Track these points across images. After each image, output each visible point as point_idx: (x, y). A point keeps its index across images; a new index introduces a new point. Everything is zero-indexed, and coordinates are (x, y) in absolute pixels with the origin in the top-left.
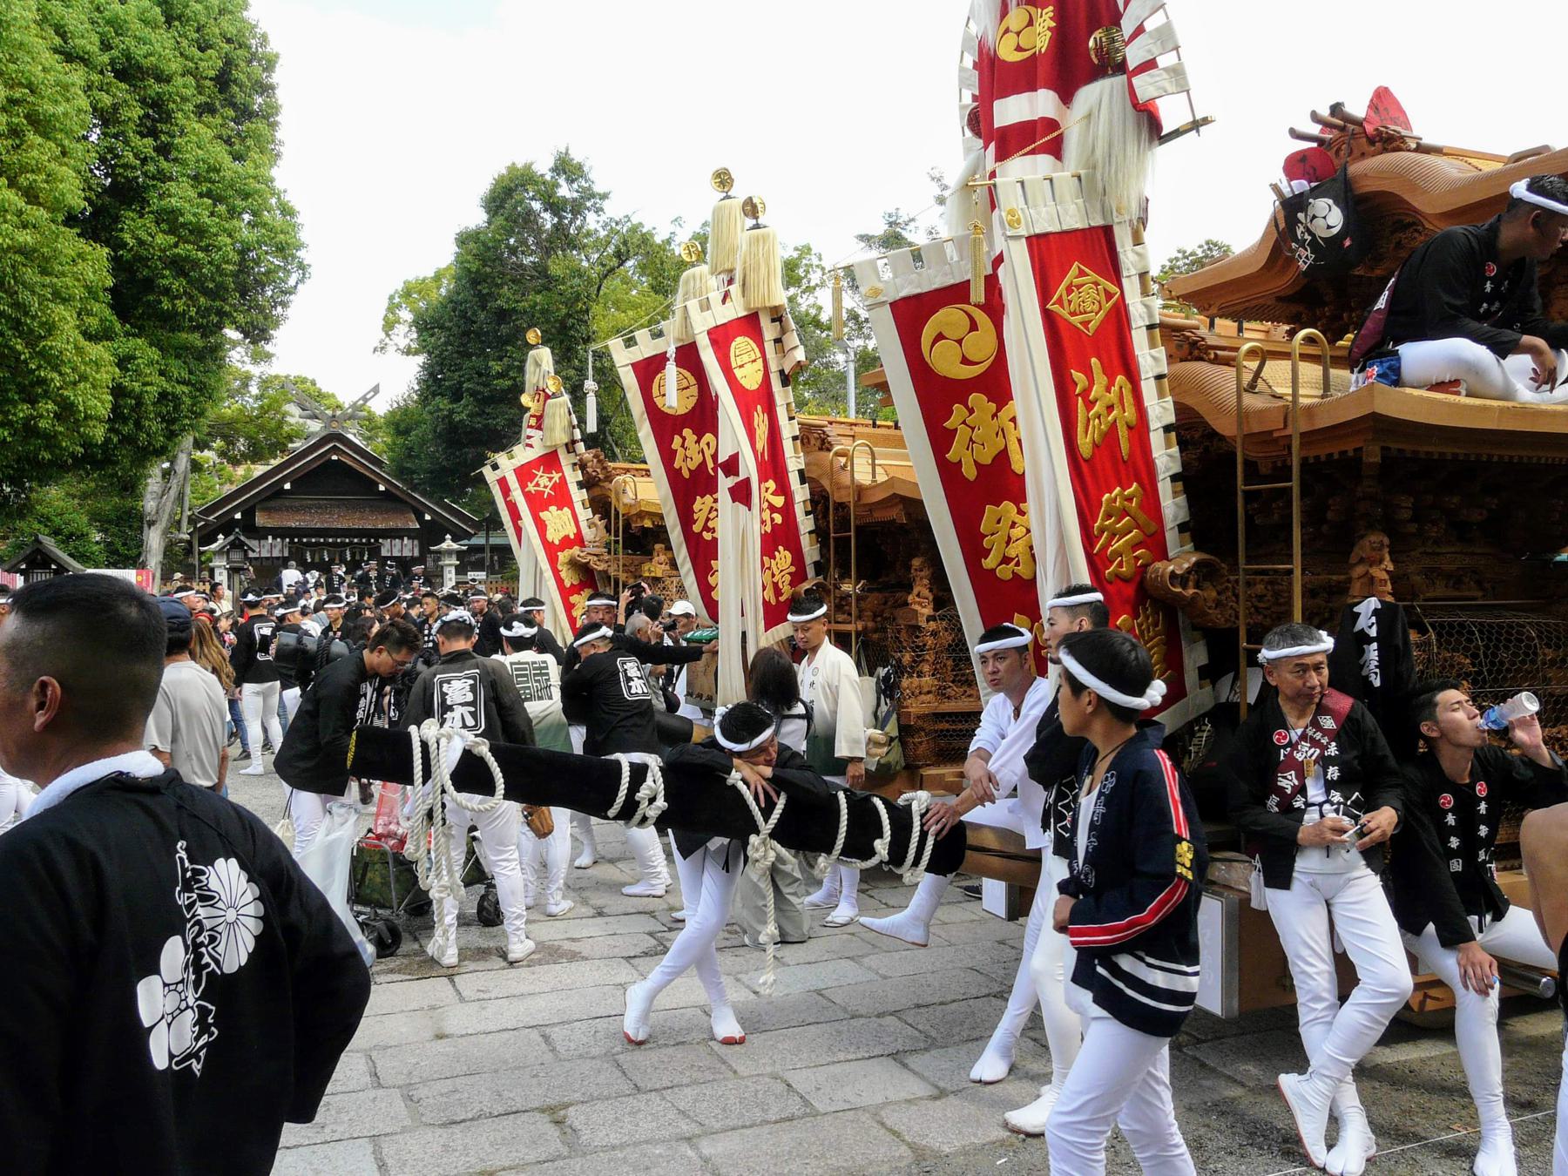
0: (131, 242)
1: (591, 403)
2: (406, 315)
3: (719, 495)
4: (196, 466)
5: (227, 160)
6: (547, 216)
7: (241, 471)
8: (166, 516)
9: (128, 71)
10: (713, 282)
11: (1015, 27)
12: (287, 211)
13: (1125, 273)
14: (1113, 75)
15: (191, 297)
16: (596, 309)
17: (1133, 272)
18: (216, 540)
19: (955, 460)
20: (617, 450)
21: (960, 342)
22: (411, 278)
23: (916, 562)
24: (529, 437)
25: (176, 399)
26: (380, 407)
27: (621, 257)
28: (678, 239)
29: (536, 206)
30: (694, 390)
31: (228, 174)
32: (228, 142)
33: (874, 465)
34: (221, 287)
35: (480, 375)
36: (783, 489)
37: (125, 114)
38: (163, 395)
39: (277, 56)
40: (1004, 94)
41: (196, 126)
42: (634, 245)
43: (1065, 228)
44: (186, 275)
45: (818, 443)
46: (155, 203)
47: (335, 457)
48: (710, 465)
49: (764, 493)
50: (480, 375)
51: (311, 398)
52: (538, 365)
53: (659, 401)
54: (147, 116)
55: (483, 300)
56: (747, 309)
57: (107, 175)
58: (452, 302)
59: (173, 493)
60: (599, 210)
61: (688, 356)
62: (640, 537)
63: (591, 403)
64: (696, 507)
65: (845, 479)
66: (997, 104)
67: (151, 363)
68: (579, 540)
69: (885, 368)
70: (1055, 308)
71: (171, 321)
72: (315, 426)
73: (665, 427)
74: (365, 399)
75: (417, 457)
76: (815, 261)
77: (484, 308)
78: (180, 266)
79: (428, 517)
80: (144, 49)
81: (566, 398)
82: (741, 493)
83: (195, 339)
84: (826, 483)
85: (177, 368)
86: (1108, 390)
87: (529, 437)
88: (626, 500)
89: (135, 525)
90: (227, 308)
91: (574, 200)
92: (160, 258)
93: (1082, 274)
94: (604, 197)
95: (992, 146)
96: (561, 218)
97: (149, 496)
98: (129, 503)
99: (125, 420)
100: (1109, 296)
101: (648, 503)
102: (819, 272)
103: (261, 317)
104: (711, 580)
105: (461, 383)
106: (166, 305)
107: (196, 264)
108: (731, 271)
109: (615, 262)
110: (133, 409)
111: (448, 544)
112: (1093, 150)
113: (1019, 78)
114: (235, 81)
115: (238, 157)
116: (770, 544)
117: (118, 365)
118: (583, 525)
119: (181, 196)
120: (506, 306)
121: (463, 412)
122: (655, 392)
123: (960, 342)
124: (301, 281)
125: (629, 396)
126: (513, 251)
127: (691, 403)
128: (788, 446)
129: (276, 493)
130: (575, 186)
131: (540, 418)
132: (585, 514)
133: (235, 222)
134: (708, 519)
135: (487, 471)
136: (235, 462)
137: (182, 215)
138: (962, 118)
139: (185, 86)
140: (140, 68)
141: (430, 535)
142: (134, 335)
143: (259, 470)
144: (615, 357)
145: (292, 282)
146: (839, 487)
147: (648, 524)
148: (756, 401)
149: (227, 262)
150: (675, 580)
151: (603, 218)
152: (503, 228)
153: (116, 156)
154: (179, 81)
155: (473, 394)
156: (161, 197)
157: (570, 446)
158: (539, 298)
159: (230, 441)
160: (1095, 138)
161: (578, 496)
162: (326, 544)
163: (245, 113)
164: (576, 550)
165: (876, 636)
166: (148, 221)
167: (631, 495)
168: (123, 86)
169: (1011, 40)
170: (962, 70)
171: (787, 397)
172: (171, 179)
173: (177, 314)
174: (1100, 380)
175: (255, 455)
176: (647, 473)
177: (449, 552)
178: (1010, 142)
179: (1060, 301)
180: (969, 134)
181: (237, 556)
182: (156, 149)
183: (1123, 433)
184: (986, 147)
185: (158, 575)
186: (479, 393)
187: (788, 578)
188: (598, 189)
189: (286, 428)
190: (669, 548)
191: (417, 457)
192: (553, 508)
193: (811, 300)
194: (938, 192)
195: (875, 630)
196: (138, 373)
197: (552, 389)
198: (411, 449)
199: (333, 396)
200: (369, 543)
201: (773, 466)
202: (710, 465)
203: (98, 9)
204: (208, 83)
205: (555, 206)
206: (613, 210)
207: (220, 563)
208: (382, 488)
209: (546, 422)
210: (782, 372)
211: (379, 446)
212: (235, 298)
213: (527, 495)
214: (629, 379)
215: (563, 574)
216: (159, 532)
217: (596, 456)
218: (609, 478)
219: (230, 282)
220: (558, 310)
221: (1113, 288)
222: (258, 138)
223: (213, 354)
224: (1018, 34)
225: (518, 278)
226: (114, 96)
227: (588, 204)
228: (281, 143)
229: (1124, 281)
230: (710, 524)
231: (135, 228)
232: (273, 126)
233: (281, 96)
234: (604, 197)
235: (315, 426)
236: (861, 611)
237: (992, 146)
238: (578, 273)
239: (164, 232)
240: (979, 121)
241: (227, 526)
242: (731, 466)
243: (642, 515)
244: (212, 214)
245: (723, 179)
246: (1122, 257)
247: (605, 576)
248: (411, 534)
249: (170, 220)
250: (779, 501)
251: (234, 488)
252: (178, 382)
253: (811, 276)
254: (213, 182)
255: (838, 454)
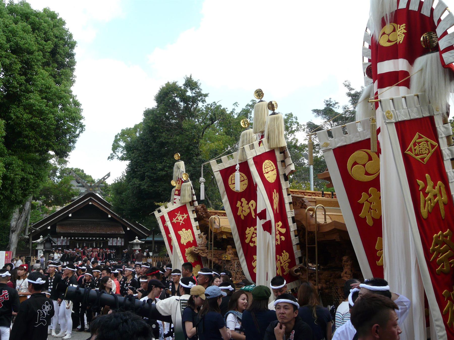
0: (14, 117)
1: (202, 187)
2: (122, 144)
3: (257, 227)
4: (33, 207)
5: (53, 84)
6: (182, 104)
7: (51, 209)
8: (19, 229)
9: (17, 50)
10: (255, 136)
11: (387, 32)
12: (77, 104)
13: (440, 136)
14: (432, 52)
15: (36, 139)
16: (201, 141)
17: (444, 135)
18: (39, 238)
19: (363, 217)
20: (210, 202)
21: (364, 165)
22: (124, 128)
23: (345, 258)
24: (175, 199)
25: (28, 180)
26: (110, 182)
27: (212, 120)
28: (236, 112)
29: (177, 99)
30: (246, 182)
31: (54, 90)
32: (54, 77)
33: (325, 215)
34: (49, 134)
35: (152, 169)
36: (285, 225)
37: (14, 67)
38: (23, 179)
39: (75, 43)
40: (383, 60)
41: (42, 71)
42: (217, 114)
43: (412, 118)
44: (35, 130)
45: (300, 205)
46: (24, 101)
47: (90, 203)
48: (253, 214)
49: (277, 227)
50: (152, 169)
51: (80, 176)
52: (179, 168)
53: (231, 187)
54: (23, 67)
55: (154, 138)
56: (270, 148)
57: (5, 91)
58: (141, 138)
59: (23, 218)
60: (203, 101)
61: (244, 167)
62: (221, 242)
63: (202, 187)
64: (247, 232)
65: (313, 221)
66: (379, 64)
67: (19, 166)
68: (194, 243)
69: (329, 171)
70: (409, 153)
71: (27, 148)
72: (83, 190)
73: (234, 197)
74: (104, 179)
75: (125, 204)
76: (294, 120)
77: (155, 141)
78: (32, 126)
79: (128, 229)
80: (23, 42)
81: (190, 182)
82: (267, 227)
83: (37, 155)
84: (304, 223)
85: (29, 168)
86: (434, 188)
87: (175, 199)
88: (215, 227)
89: (6, 232)
90: (51, 143)
91: (193, 97)
92: (25, 123)
93: (420, 137)
94: (206, 95)
95: (376, 82)
96: (188, 104)
97: (13, 220)
98: (4, 222)
99: (6, 189)
100: (433, 146)
101: (225, 228)
102: (296, 125)
103: (64, 147)
104: (253, 264)
105: (144, 173)
106: (27, 142)
107: (39, 126)
108: (263, 132)
109: (209, 122)
110: (10, 185)
111: (137, 240)
112: (424, 84)
113: (391, 53)
114: (58, 53)
115: (58, 83)
116: (279, 250)
117: (5, 167)
118: (197, 237)
119: (35, 99)
120: (164, 141)
121: (145, 185)
122: (230, 182)
123: (364, 165)
124: (81, 132)
125: (219, 184)
126: (167, 118)
127: (245, 187)
128: (287, 207)
129: (66, 217)
130: (194, 91)
131: (179, 191)
132: (197, 232)
133: (55, 109)
134: (252, 237)
135: (156, 213)
136: (50, 205)
137: (35, 106)
138: (364, 69)
139: (38, 55)
140: (21, 48)
141: (129, 236)
142: (12, 155)
143: (59, 208)
144: (213, 168)
145: (77, 132)
146: (310, 225)
147: (224, 237)
148: (273, 188)
149: (52, 125)
150: (236, 261)
151: (205, 104)
152: (163, 108)
153: (9, 83)
154: (36, 53)
155: (149, 177)
156: (27, 99)
157: (192, 203)
158: (178, 137)
159: (47, 197)
160: (424, 79)
161: (195, 224)
162: (85, 240)
163: (61, 65)
164: (193, 248)
165: (327, 291)
166: (21, 109)
167: (217, 224)
168: (15, 56)
169: (386, 37)
170: (364, 49)
171: (287, 185)
172: (32, 92)
173: (31, 145)
174: (430, 184)
175: (58, 202)
176: (225, 214)
177: (137, 244)
178: (387, 80)
179: (411, 150)
180: (366, 76)
181: (48, 245)
182: (25, 80)
183: (442, 207)
184: (374, 82)
185: (14, 253)
186: (152, 177)
187: (287, 264)
188: (203, 92)
189: (71, 191)
190: (234, 247)
191: (125, 204)
192: (184, 230)
193: (293, 136)
194: (348, 91)
195: (327, 288)
196: (13, 170)
197: (184, 179)
198: (123, 200)
199: (90, 177)
200: (103, 240)
201: (281, 215)
202: (253, 214)
203: (6, 26)
204: (48, 54)
205: (185, 99)
206: (209, 100)
207: (40, 248)
208: (109, 216)
209: (182, 193)
210: (284, 175)
211: (109, 198)
212: (54, 139)
213: (173, 224)
214: (218, 177)
215: (187, 258)
216: (16, 235)
217: (202, 207)
218: (208, 217)
219: (53, 132)
220: (186, 142)
221: (434, 143)
222: (66, 74)
223: (43, 162)
224: (388, 35)
225: (170, 129)
226: (11, 60)
227: (199, 99)
228: (75, 77)
229: (440, 140)
230: (253, 240)
231: (16, 112)
232: (73, 70)
233: (76, 58)
234: (206, 95)
235: (83, 190)
236: (320, 279)
237: (376, 82)
238: (195, 127)
239: (27, 113)
240: (371, 71)
241: (44, 232)
242: (263, 215)
243: (222, 233)
244: (47, 106)
245: (259, 93)
246: (438, 129)
247: (206, 259)
248: (121, 236)
249: (30, 108)
250: (283, 231)
251: (48, 216)
252: (29, 174)
253: (293, 126)
254: (48, 93)
255: (310, 210)
